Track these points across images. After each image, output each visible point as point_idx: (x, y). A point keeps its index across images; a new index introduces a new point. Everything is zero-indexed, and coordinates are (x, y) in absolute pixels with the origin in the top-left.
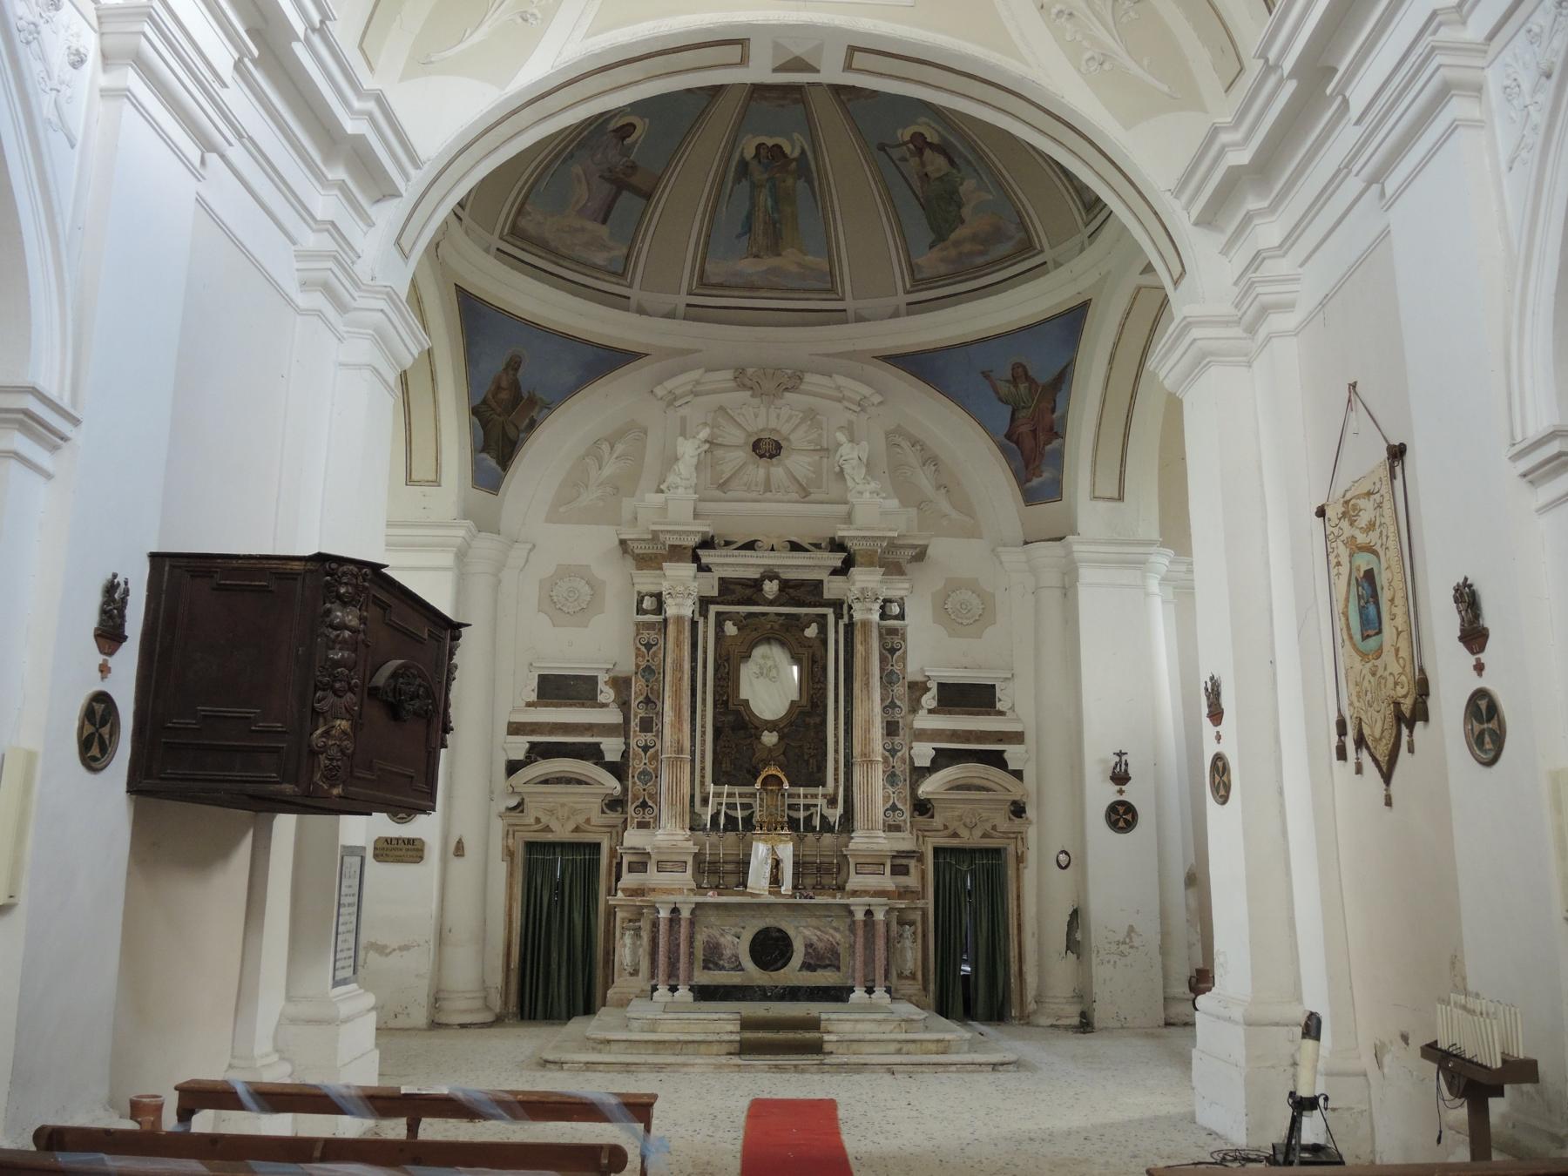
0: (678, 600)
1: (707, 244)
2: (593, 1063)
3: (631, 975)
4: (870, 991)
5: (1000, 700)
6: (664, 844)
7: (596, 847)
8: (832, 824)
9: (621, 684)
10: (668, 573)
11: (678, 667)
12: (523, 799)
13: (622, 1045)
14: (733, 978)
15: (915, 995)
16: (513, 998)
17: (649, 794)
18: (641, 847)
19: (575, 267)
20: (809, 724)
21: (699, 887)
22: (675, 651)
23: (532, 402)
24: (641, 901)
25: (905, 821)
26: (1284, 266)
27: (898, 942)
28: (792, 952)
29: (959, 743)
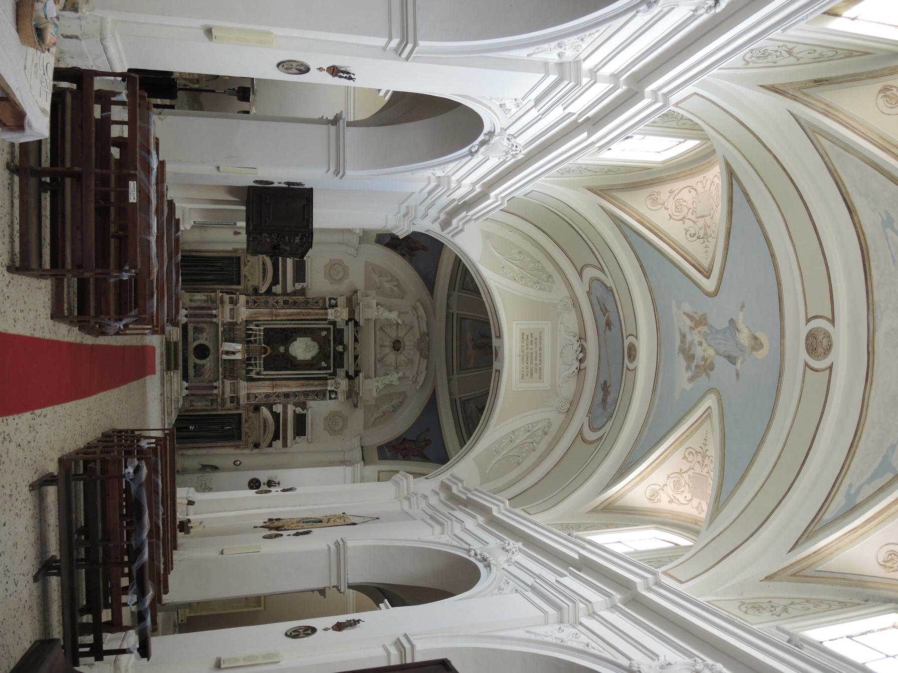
3: (190, 299)
4: (187, 388)
6: (240, 310)
7: (239, 283)
9: (302, 292)
10: (344, 309)
11: (309, 314)
14: (190, 338)
21: (224, 324)
22: (315, 313)
26: (423, 505)
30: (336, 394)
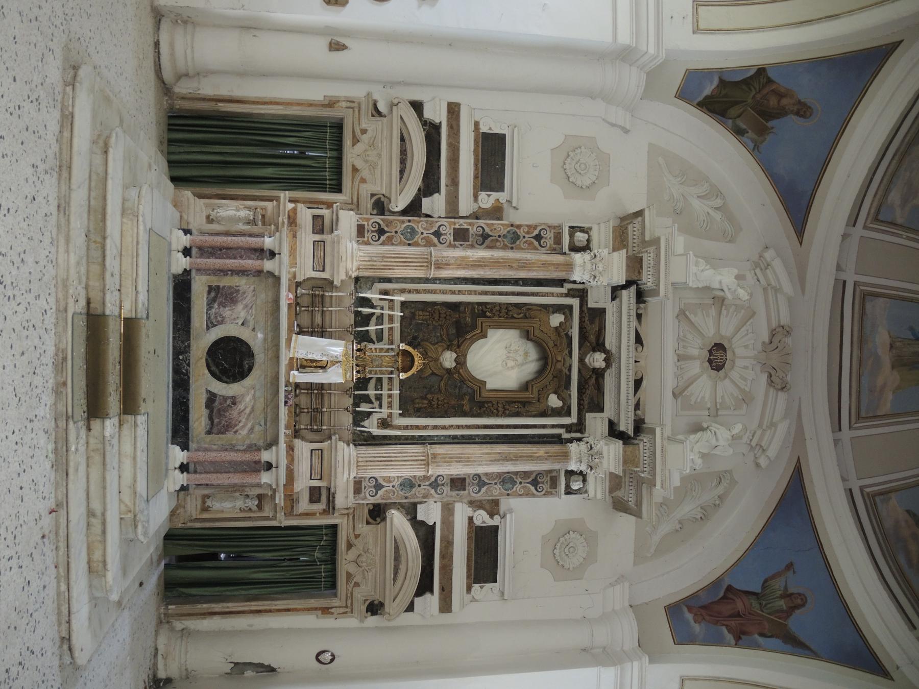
0: (589, 266)
1: (904, 299)
2: (72, 124)
3: (208, 217)
4: (183, 468)
5: (482, 587)
6: (342, 249)
7: (338, 189)
8: (362, 424)
10: (616, 254)
12: (385, 117)
13: (101, 169)
15: (185, 511)
16: (188, 105)
17: (392, 237)
18: (339, 227)
19: (890, 171)
20: (463, 399)
21: (298, 284)
23: (762, 131)
24: (283, 223)
25: (365, 498)
28: (226, 382)
29: (441, 549)
30: (584, 480)
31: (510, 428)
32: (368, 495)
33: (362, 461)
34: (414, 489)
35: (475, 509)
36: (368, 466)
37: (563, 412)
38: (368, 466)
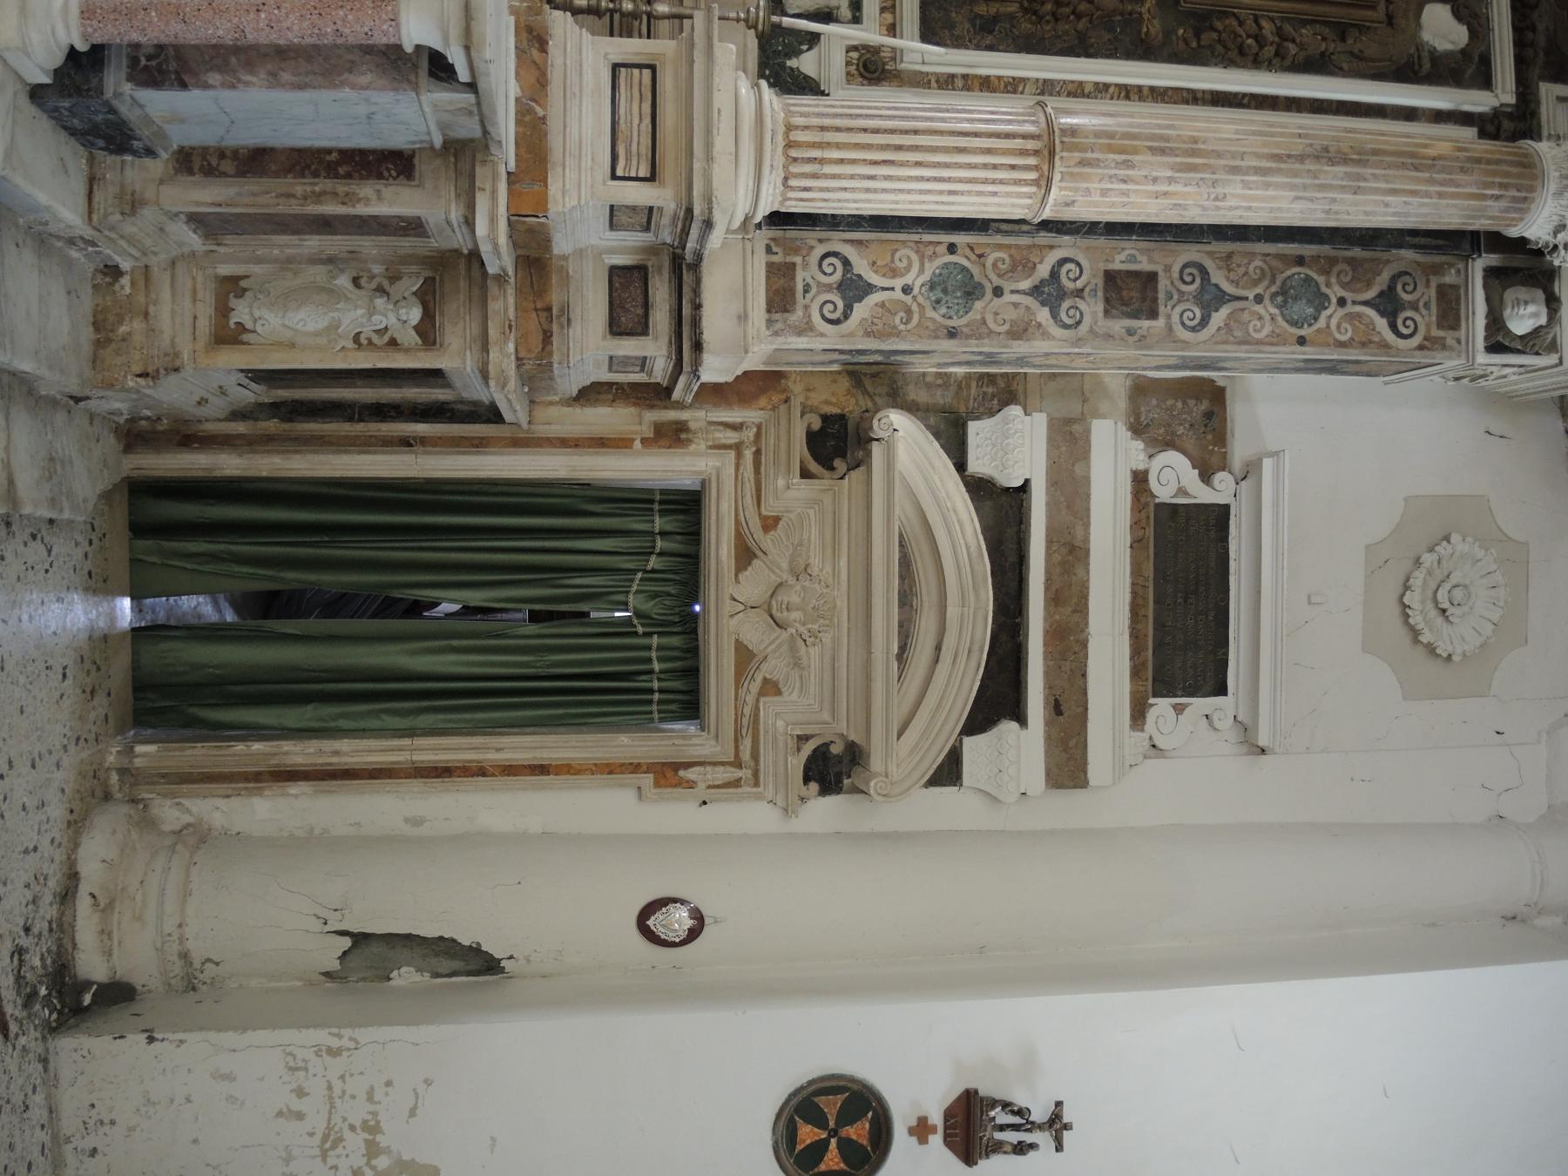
5: (1179, 709)
15: (151, 331)
27: (356, 281)
31: (1299, 111)
32: (816, 319)
33: (806, 128)
34: (978, 305)
35: (1152, 451)
36: (828, 145)
37: (1469, 72)
38: (828, 145)
